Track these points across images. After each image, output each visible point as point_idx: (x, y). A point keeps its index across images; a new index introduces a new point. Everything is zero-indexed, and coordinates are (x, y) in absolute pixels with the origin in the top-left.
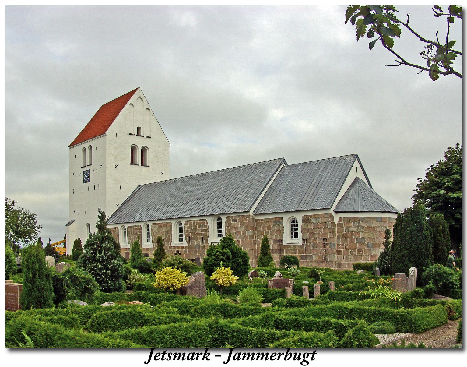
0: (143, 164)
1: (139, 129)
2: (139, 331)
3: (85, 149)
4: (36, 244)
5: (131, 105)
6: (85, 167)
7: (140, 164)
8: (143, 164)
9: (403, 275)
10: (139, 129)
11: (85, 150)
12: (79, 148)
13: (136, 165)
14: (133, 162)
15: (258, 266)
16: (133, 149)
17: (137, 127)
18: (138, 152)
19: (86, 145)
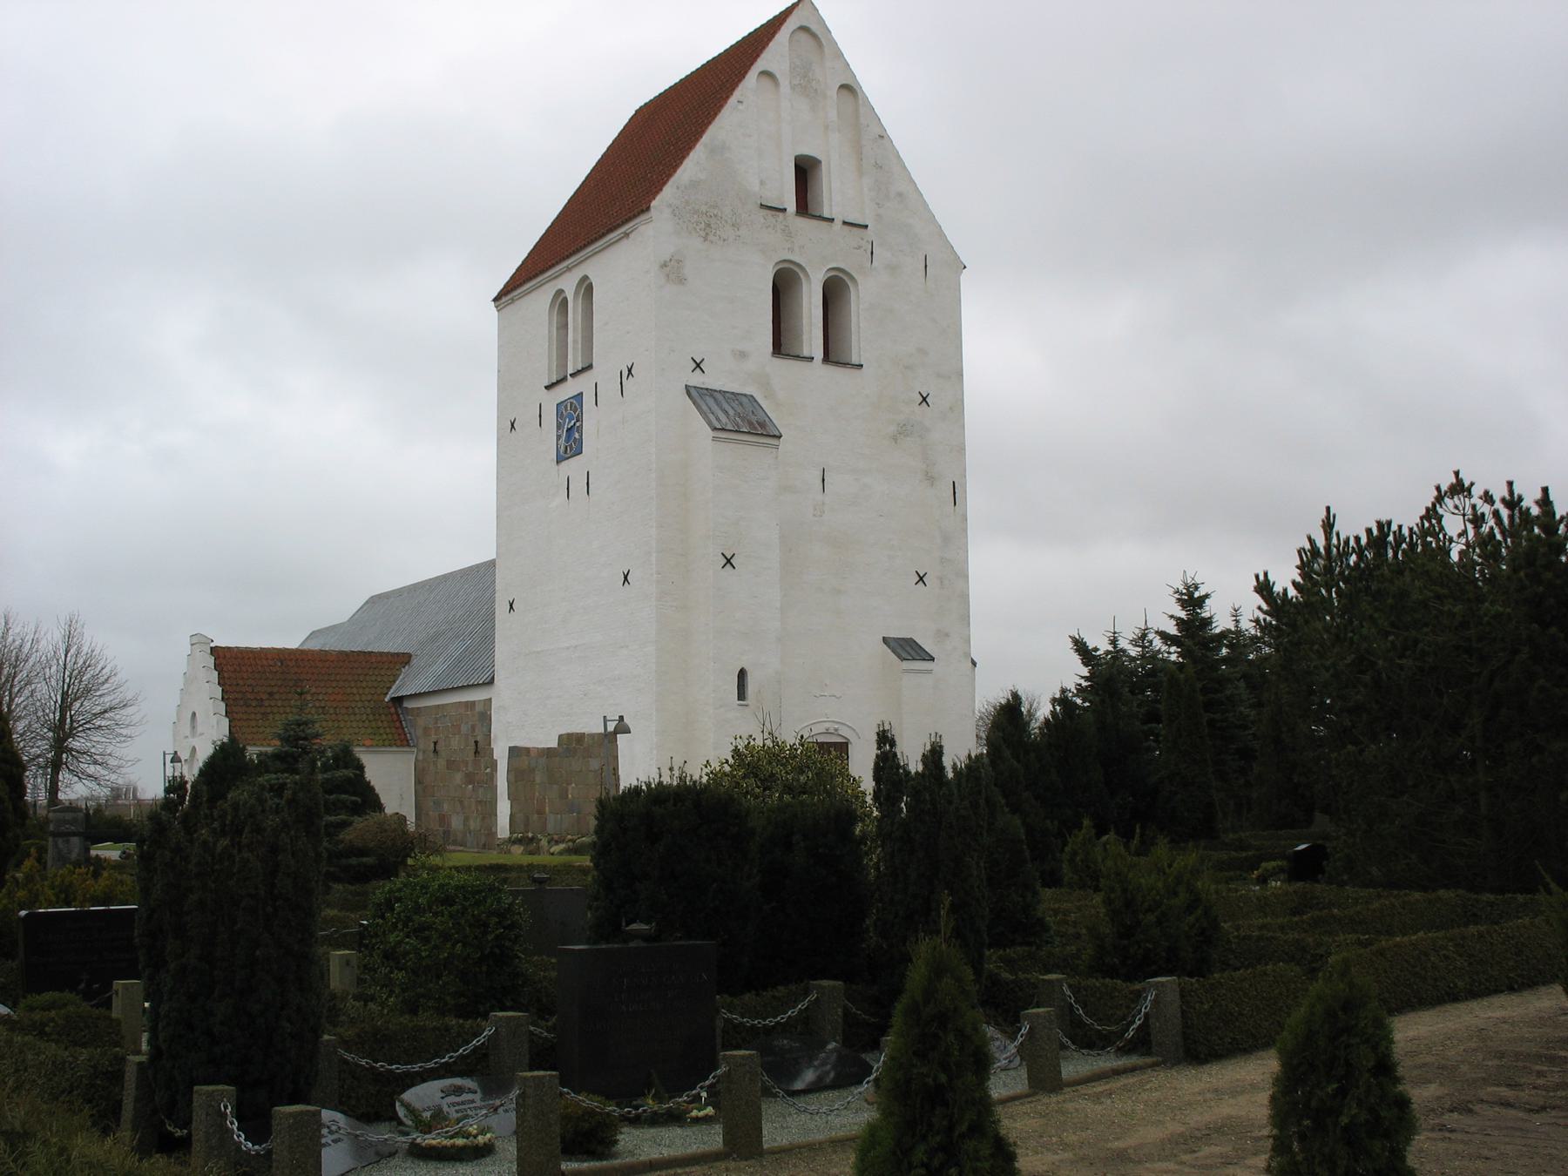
0: (830, 355)
1: (805, 171)
2: (736, 1001)
3: (565, 301)
4: (1038, 739)
5: (845, 92)
6: (564, 380)
7: (819, 354)
8: (830, 355)
9: (233, 1090)
10: (805, 171)
11: (561, 303)
12: (538, 301)
13: (798, 357)
14: (781, 344)
15: (514, 752)
16: (784, 286)
17: (797, 158)
18: (810, 297)
19: (568, 283)
